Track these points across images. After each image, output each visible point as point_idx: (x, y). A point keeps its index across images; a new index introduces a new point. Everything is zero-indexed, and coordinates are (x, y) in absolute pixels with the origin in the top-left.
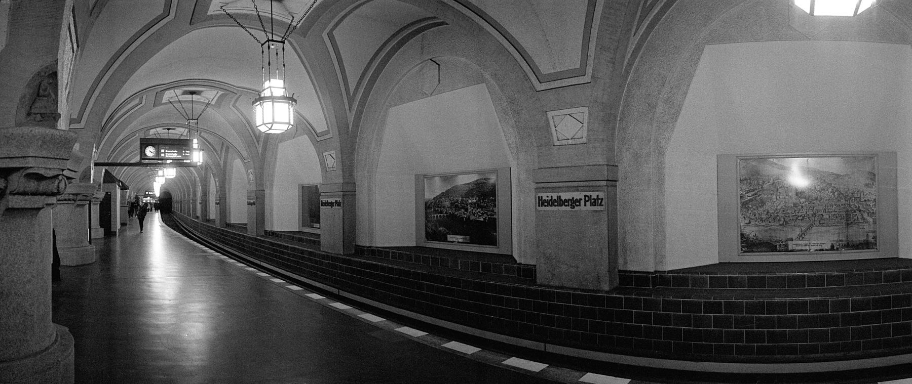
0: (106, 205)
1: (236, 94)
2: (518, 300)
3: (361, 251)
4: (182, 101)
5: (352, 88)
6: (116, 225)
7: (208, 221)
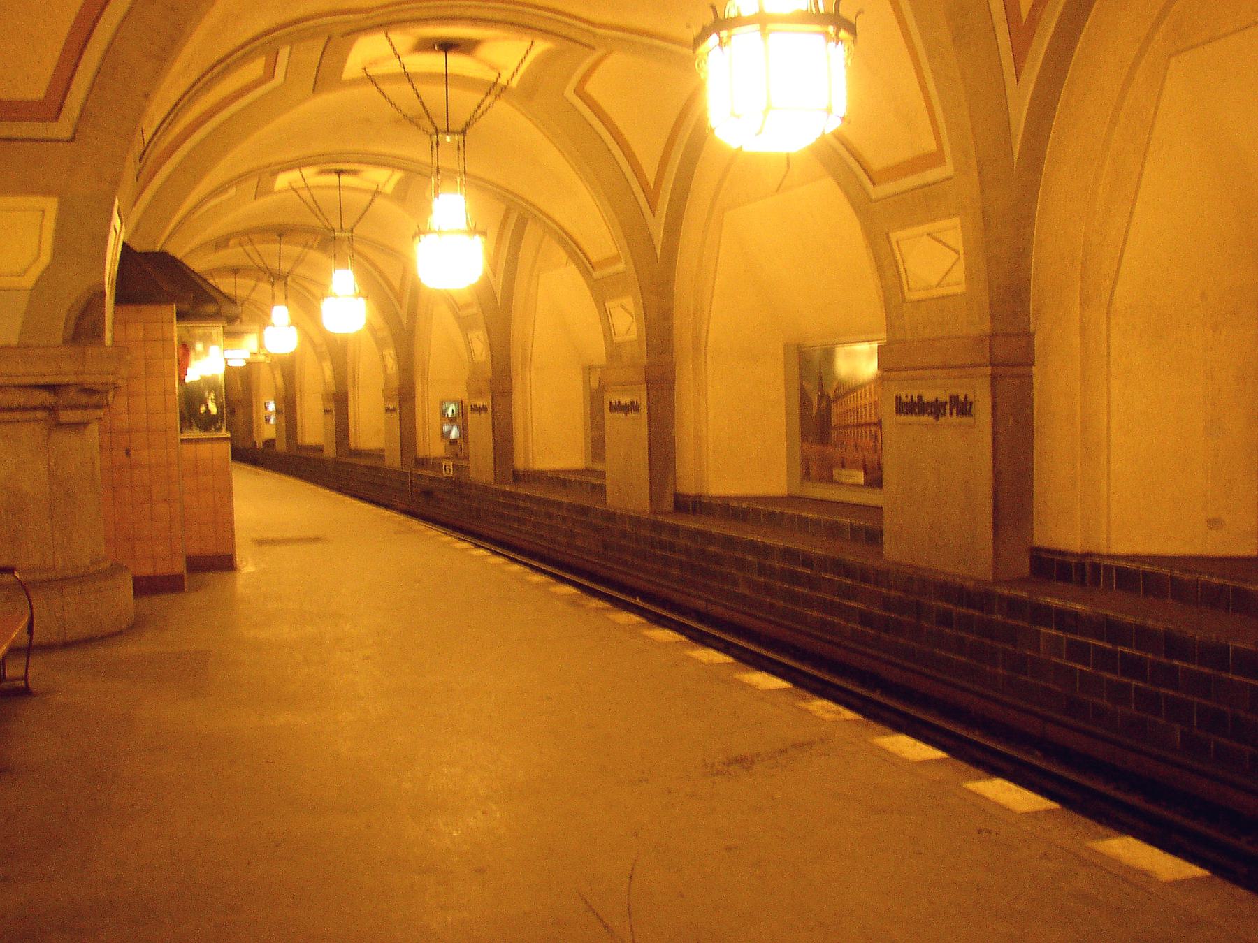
1: (594, 49)
4: (415, 74)
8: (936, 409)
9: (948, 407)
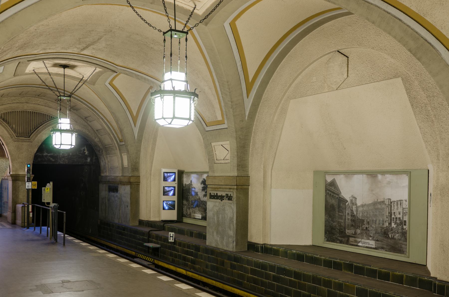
2: (404, 284)
8: (222, 198)
9: (225, 197)
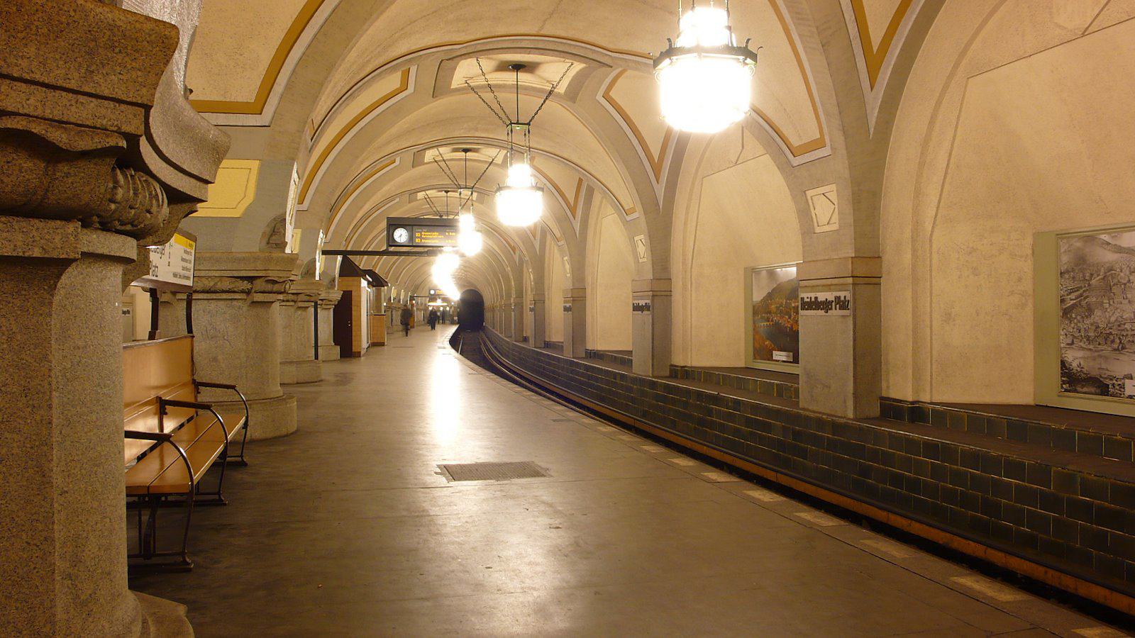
0: (344, 311)
3: (893, 410)
5: (876, 37)
6: (360, 341)
7: (548, 345)
9: (834, 304)
